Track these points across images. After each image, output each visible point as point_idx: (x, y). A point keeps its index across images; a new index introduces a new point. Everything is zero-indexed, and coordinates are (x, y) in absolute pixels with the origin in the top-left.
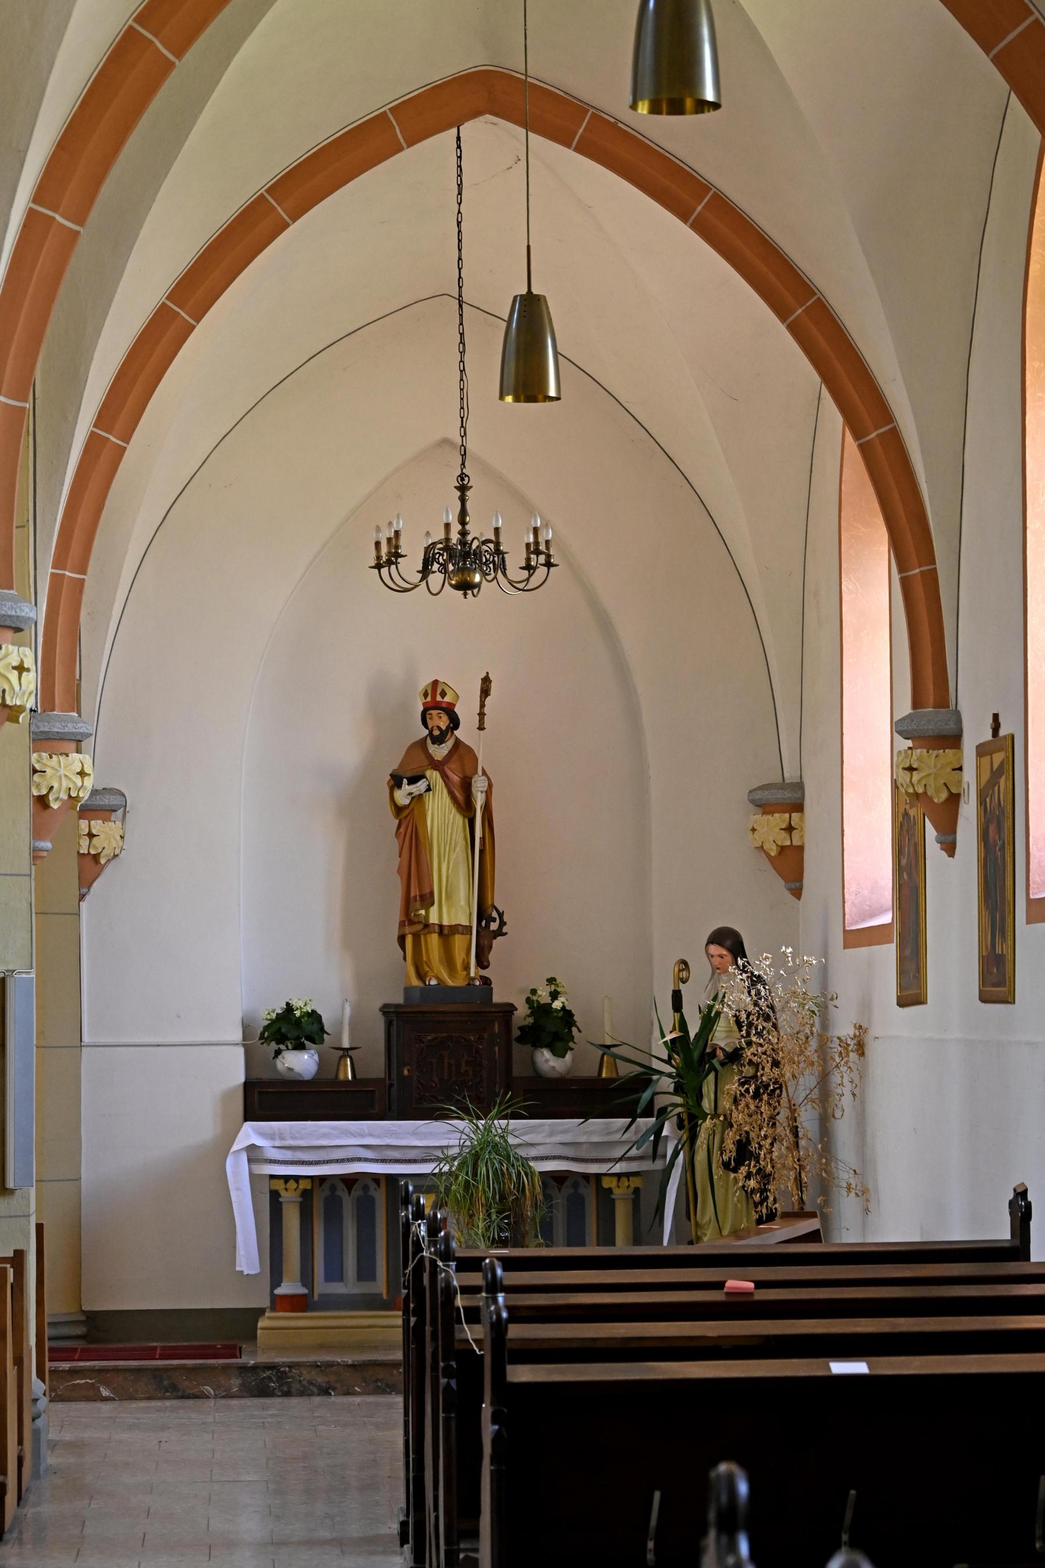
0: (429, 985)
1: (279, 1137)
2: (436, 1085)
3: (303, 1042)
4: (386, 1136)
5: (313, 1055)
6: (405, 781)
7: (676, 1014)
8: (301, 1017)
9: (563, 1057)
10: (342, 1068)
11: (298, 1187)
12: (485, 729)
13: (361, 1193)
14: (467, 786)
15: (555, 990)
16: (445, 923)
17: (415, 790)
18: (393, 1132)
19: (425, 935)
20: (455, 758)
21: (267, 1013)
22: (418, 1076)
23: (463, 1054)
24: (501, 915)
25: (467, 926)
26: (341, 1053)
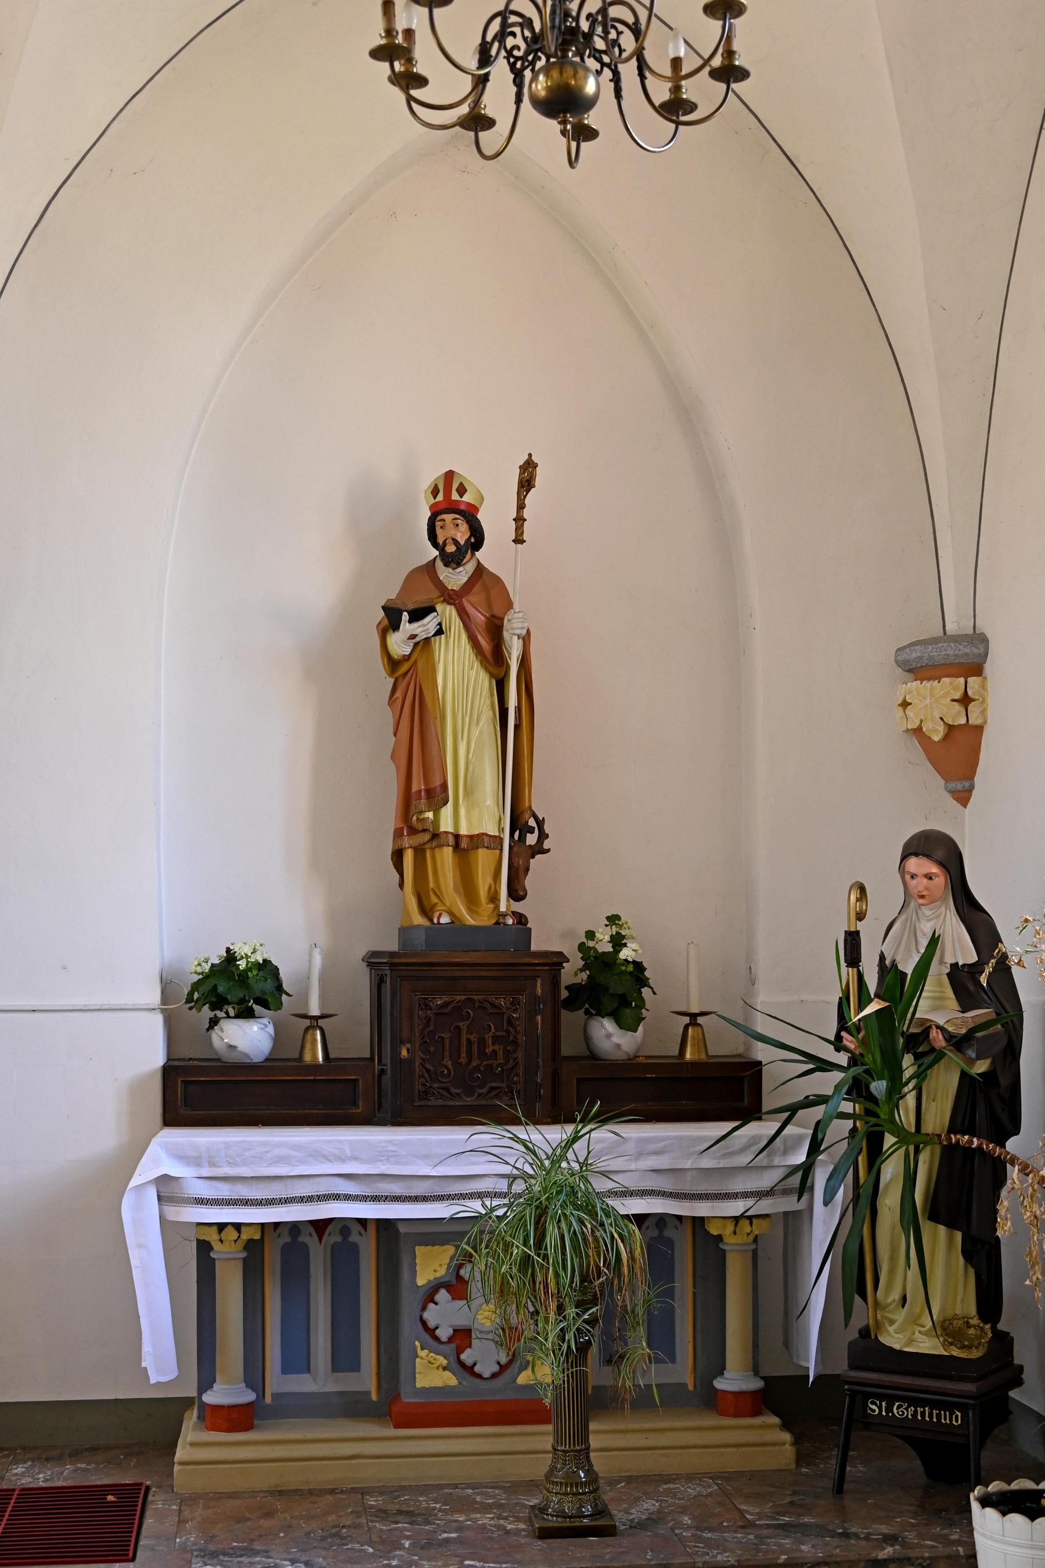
0: (439, 923)
1: (209, 1162)
2: (449, 1070)
3: (251, 1007)
4: (381, 1161)
5: (266, 1026)
6: (405, 616)
7: (850, 969)
8: (248, 969)
9: (635, 1031)
10: (308, 1046)
11: (239, 1237)
12: (525, 541)
13: (339, 1239)
14: (495, 629)
15: (617, 933)
16: (464, 831)
17: (420, 630)
18: (390, 1154)
19: (432, 849)
20: (478, 588)
21: (196, 963)
22: (423, 1060)
23: (490, 1026)
24: (540, 823)
25: (495, 837)
26: (307, 1023)
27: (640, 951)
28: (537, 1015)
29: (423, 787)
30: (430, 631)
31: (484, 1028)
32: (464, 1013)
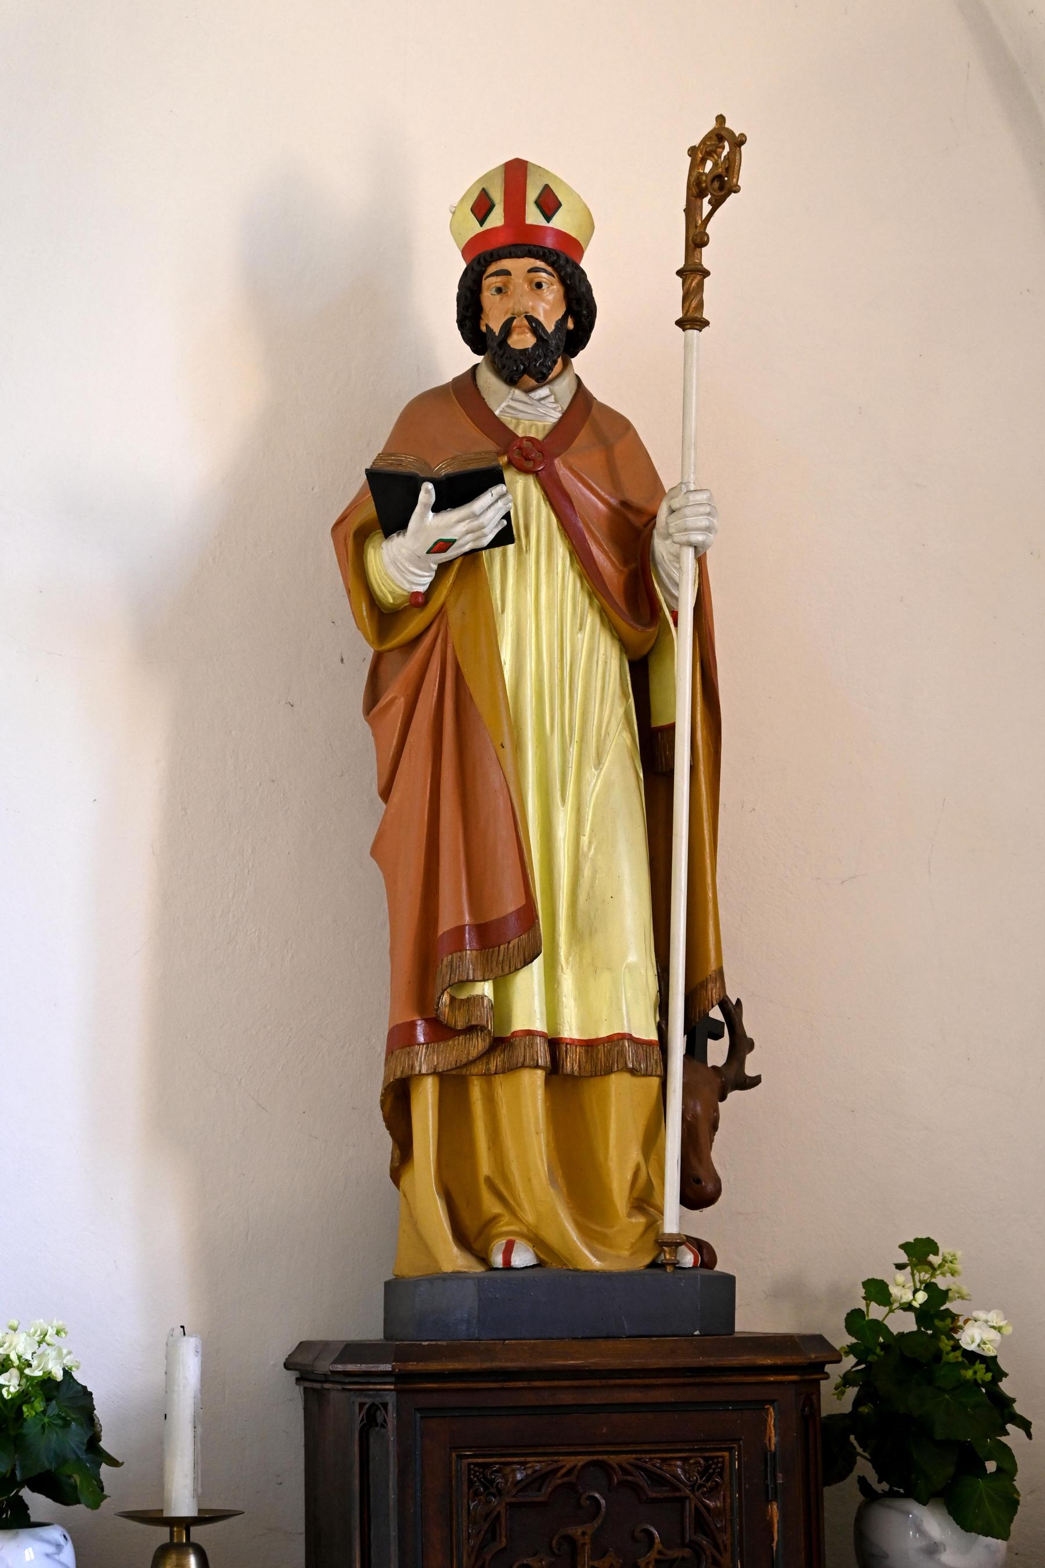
0: (508, 1266)
6: (427, 494)
8: (23, 1397)
12: (706, 323)
16: (570, 1030)
17: (462, 527)
19: (487, 1076)
23: (650, 1535)
26: (162, 1535)
27: (1008, 1330)
28: (768, 1501)
29: (467, 919)
30: (486, 531)
31: (634, 1539)
32: (585, 1503)
